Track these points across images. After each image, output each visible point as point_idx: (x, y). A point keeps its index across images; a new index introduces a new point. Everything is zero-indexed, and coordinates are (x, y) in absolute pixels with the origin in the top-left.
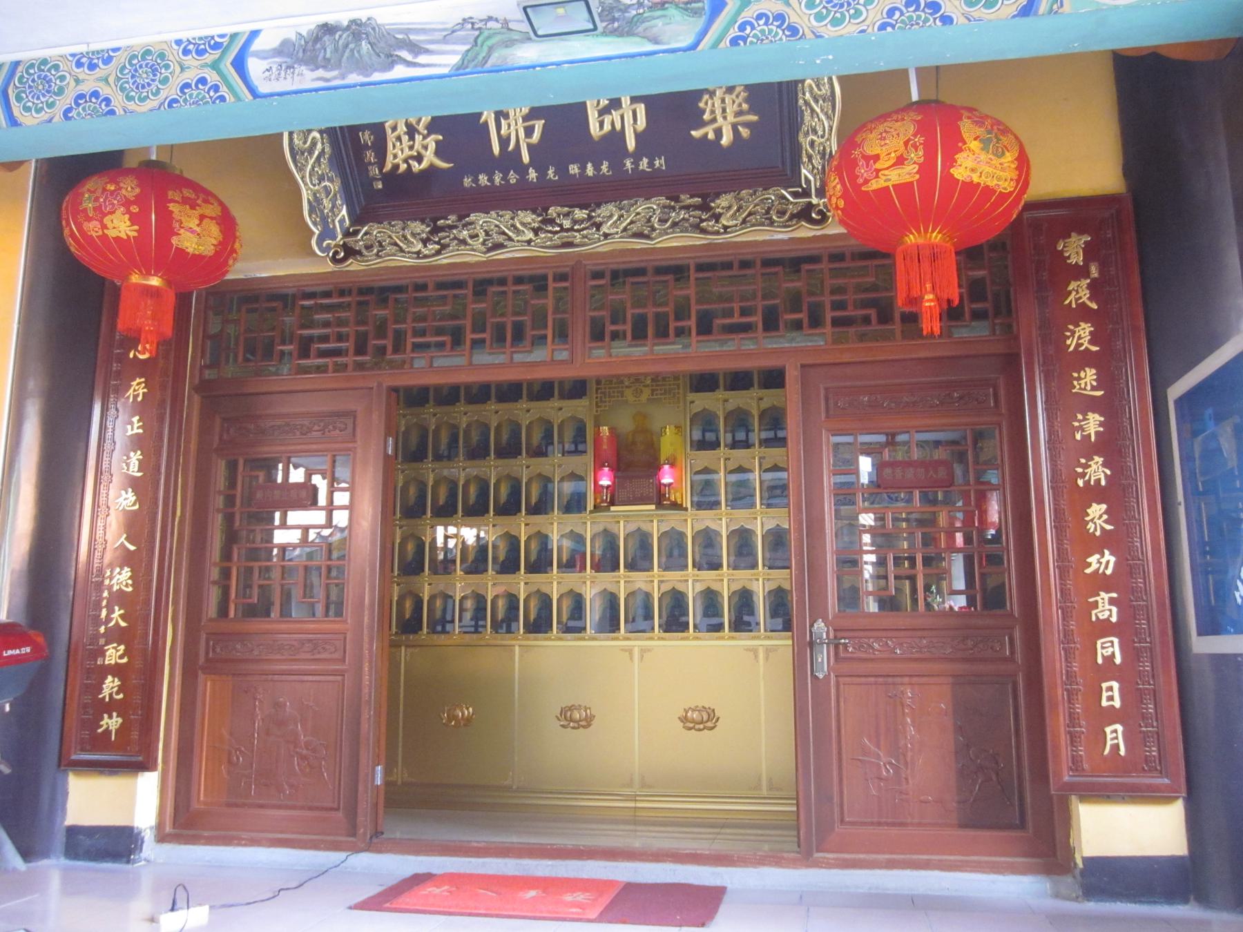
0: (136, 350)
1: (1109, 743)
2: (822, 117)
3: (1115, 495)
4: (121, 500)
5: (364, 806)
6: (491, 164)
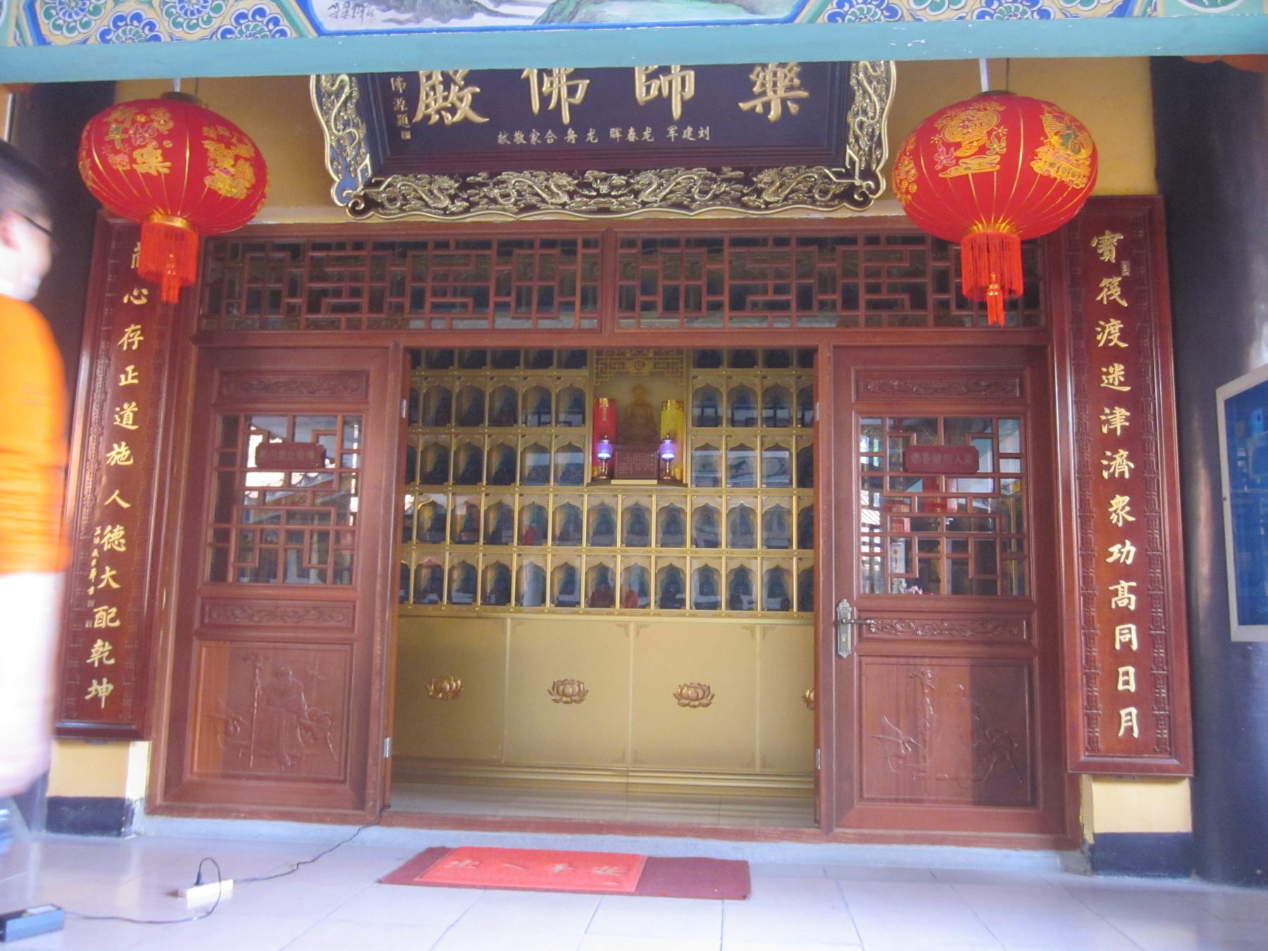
0: (131, 294)
1: (1124, 725)
2: (875, 99)
3: (1138, 487)
4: (113, 453)
5: (375, 777)
6: (526, 121)
